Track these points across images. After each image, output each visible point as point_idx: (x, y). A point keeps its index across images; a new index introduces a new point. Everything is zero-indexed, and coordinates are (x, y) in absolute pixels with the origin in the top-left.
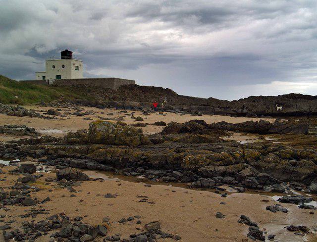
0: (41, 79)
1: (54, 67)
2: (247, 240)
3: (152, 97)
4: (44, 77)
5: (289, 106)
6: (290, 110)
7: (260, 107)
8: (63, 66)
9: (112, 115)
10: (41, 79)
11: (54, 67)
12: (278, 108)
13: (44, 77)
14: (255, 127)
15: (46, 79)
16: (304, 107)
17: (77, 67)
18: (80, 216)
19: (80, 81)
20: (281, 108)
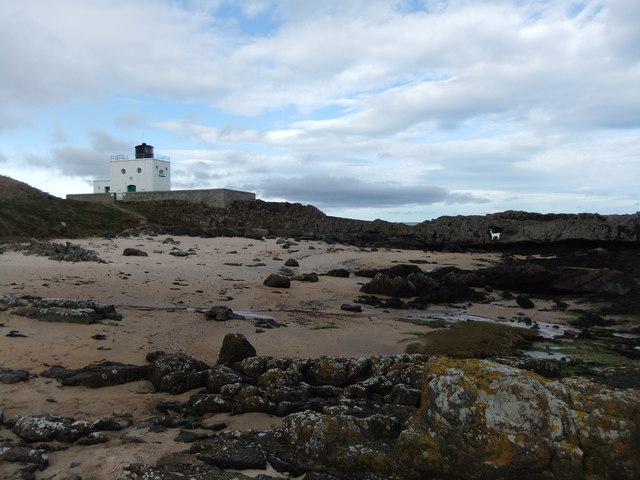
0: (103, 191)
1: (124, 171)
2: (186, 469)
3: (287, 220)
4: (108, 188)
5: (512, 233)
6: (513, 239)
7: (463, 235)
8: (139, 170)
9: (129, 252)
10: (103, 191)
11: (124, 171)
12: (493, 235)
13: (108, 188)
14: (356, 460)
15: (110, 191)
16: (537, 233)
17: (161, 171)
18: (328, 255)
19: (551, 225)
20: (498, 235)
